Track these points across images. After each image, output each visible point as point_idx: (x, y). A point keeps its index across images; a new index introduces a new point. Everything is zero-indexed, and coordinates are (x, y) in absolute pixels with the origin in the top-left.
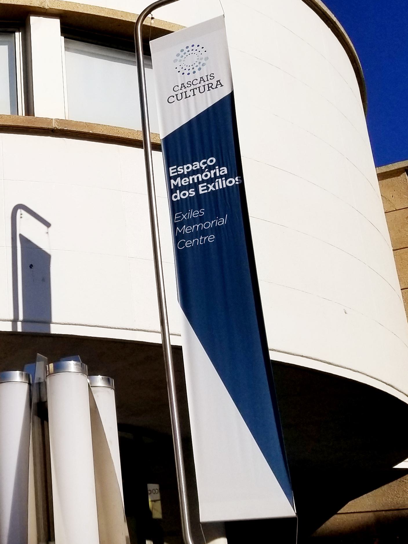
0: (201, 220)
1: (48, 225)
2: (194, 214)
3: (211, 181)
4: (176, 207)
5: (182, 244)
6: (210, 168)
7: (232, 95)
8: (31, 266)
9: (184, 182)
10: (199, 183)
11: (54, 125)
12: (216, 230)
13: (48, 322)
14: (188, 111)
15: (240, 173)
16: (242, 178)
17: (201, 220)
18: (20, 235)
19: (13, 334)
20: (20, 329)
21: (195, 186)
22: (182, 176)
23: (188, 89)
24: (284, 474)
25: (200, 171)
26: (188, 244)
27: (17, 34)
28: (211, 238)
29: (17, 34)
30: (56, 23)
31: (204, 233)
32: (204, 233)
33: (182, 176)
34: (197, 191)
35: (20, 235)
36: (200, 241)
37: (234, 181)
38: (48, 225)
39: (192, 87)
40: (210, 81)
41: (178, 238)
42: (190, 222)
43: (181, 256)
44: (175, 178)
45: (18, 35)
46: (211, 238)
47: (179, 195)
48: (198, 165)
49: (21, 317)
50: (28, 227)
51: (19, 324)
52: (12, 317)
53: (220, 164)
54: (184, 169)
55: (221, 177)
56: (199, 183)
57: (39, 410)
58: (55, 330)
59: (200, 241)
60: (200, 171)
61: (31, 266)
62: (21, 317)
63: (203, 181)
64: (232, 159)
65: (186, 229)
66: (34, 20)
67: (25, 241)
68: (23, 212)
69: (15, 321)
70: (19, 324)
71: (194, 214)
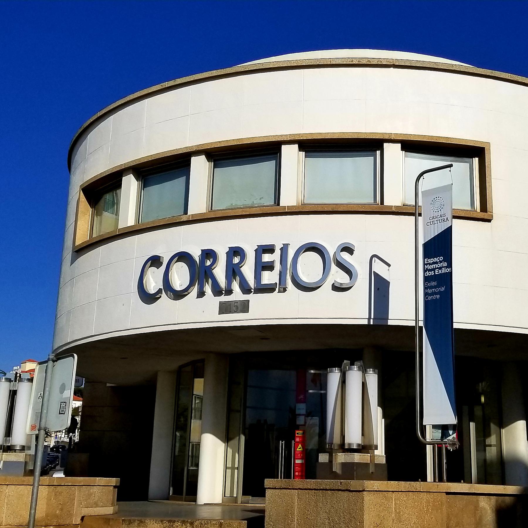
1: (389, 265)
3: (440, 268)
4: (426, 279)
5: (427, 298)
6: (441, 262)
8: (378, 289)
9: (430, 267)
10: (436, 269)
12: (440, 293)
13: (387, 319)
16: (452, 269)
17: (435, 287)
19: (369, 325)
20: (372, 323)
21: (434, 270)
22: (430, 264)
23: (435, 220)
25: (436, 263)
26: (430, 298)
27: (378, 152)
29: (378, 152)
31: (435, 293)
32: (435, 293)
33: (430, 264)
34: (435, 272)
36: (434, 297)
38: (389, 265)
39: (437, 219)
41: (426, 294)
42: (431, 287)
43: (426, 303)
44: (427, 264)
46: (438, 296)
48: (436, 260)
49: (372, 317)
50: (379, 268)
51: (372, 320)
53: (444, 260)
54: (431, 261)
55: (444, 267)
56: (436, 269)
57: (13, 394)
58: (390, 323)
59: (434, 297)
60: (436, 263)
61: (378, 289)
62: (372, 317)
64: (448, 259)
65: (429, 291)
66: (385, 145)
68: (376, 259)
69: (369, 319)
70: (372, 320)
71: (434, 284)
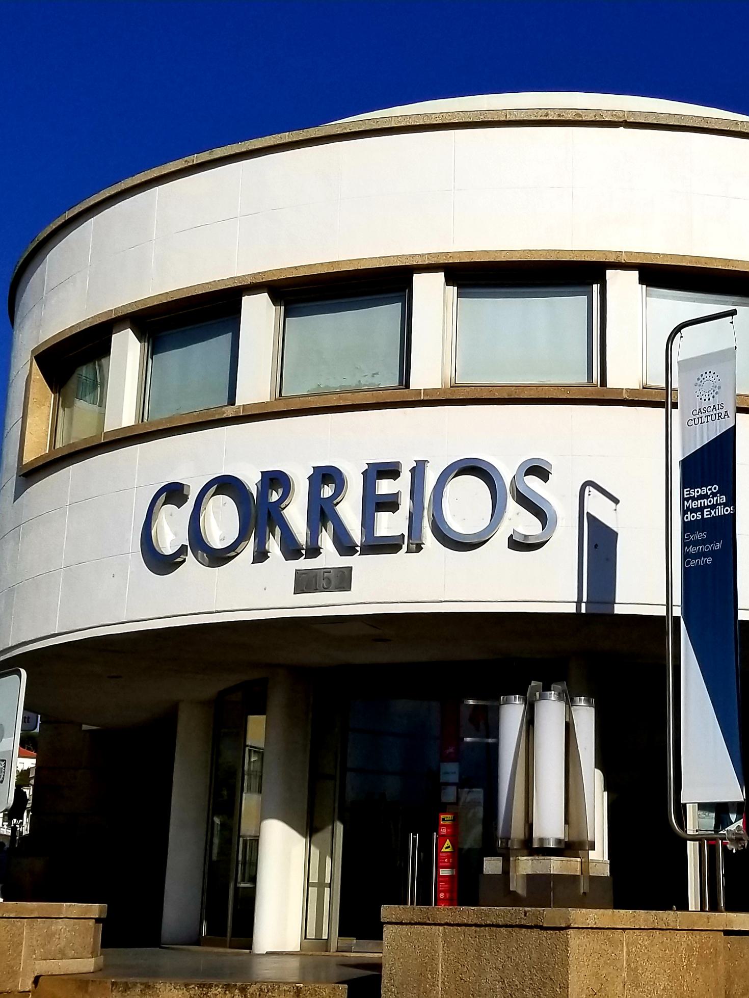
0: (703, 542)
1: (616, 501)
2: (700, 536)
3: (713, 507)
4: (687, 527)
5: (688, 563)
6: (714, 495)
7: (734, 426)
8: (596, 546)
10: (705, 507)
11: (625, 396)
12: (712, 553)
14: (695, 445)
15: (734, 504)
16: (735, 509)
17: (703, 542)
18: (588, 513)
21: (701, 510)
22: (693, 499)
23: (704, 415)
24: (739, 764)
25: (706, 496)
26: (693, 563)
27: (595, 286)
28: (709, 560)
29: (595, 286)
30: (636, 274)
31: (705, 554)
32: (705, 554)
33: (693, 499)
34: (702, 515)
35: (588, 513)
36: (701, 561)
37: (730, 510)
38: (616, 501)
39: (707, 414)
40: (720, 411)
41: (686, 556)
42: (696, 543)
43: (687, 573)
45: (596, 288)
47: (690, 517)
48: (705, 490)
49: (585, 599)
50: (597, 505)
51: (583, 605)
52: (576, 600)
53: (720, 492)
54: (695, 493)
55: (720, 504)
56: (705, 507)
58: (618, 610)
59: (701, 561)
60: (706, 496)
61: (596, 546)
62: (585, 599)
63: (708, 507)
65: (692, 550)
66: (609, 273)
67: (592, 519)
68: (591, 489)
69: (579, 602)
70: (583, 605)
71: (700, 536)
